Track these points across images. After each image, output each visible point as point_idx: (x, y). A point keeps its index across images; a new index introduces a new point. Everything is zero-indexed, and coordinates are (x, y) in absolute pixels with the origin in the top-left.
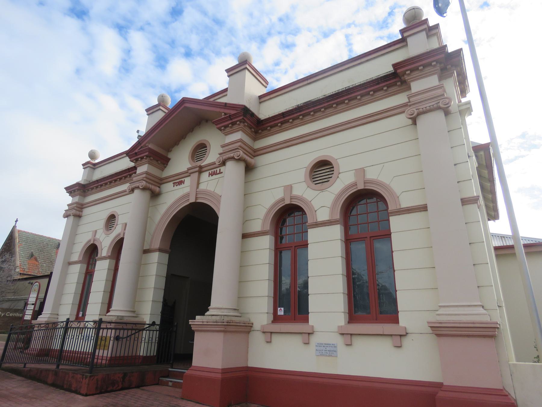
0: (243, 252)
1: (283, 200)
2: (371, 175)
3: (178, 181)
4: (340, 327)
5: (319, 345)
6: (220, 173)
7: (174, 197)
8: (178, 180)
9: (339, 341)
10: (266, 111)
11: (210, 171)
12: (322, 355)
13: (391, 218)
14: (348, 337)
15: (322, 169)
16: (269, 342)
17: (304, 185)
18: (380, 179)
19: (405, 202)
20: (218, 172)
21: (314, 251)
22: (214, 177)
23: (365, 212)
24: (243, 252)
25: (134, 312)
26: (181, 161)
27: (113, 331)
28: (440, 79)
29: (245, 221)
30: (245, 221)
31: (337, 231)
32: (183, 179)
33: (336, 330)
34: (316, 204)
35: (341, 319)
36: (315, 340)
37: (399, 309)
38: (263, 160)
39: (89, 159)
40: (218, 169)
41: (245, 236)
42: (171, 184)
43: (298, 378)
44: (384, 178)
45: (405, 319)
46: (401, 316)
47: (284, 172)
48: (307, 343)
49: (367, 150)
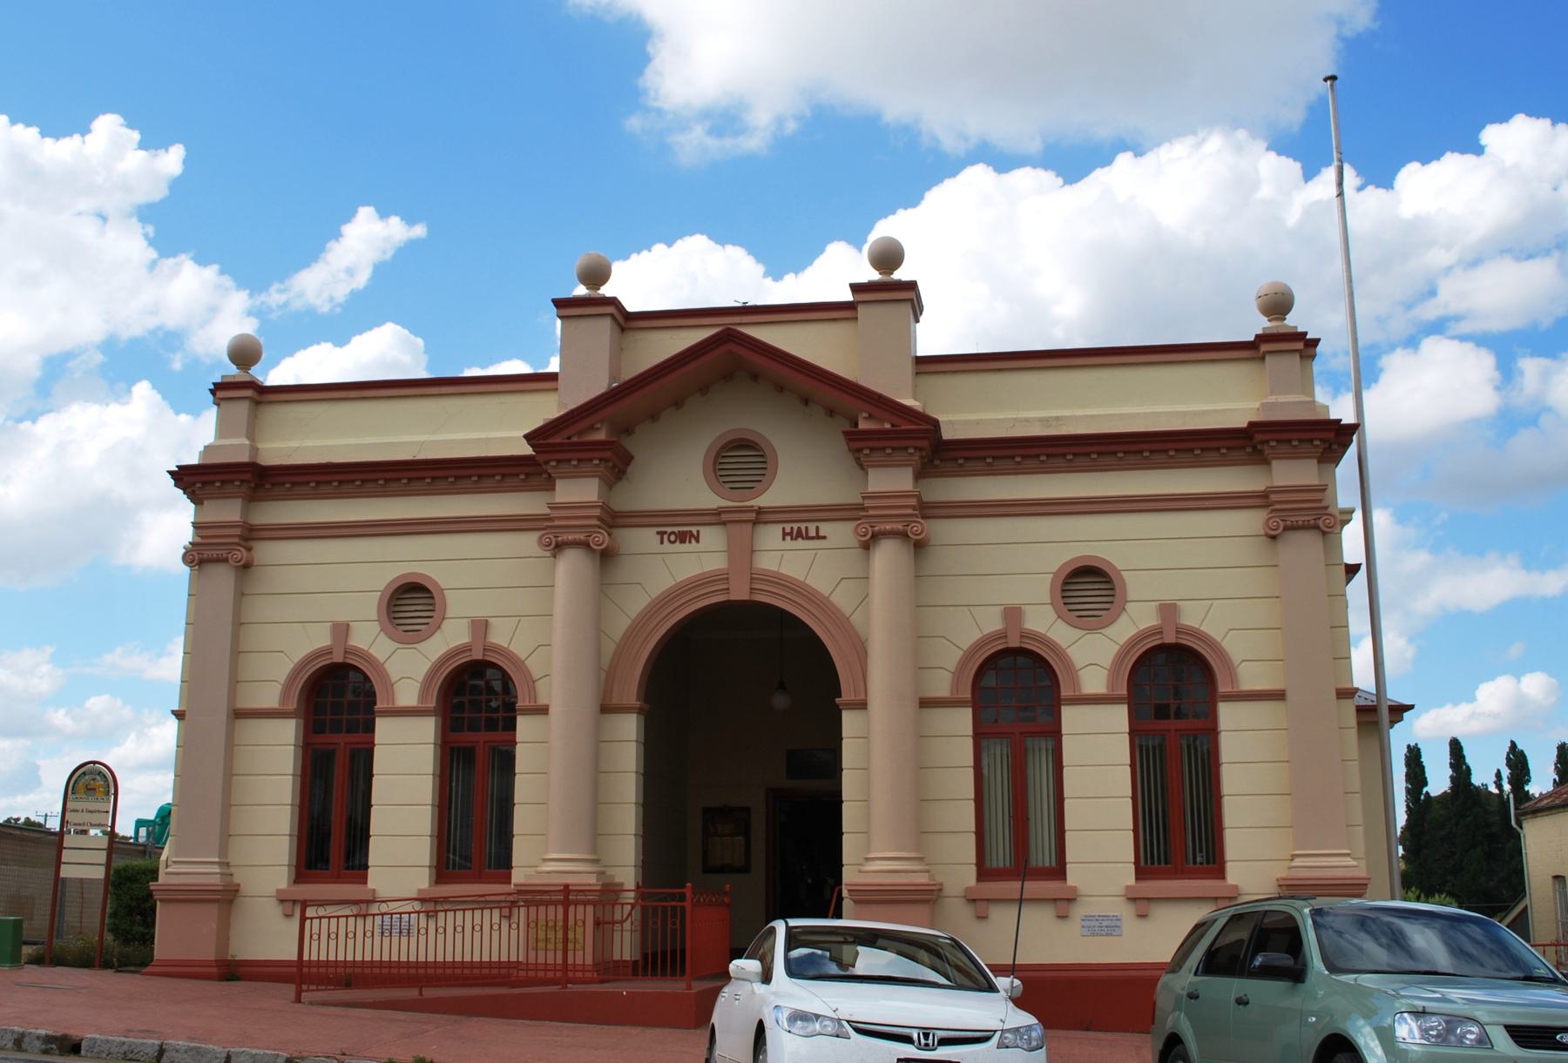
0: (921, 737)
1: (466, 649)
2: (1191, 617)
3: (676, 529)
4: (968, 889)
5: (1088, 918)
6: (818, 537)
7: (672, 572)
8: (680, 527)
9: (1126, 912)
10: (966, 414)
11: (788, 527)
12: (1093, 935)
13: (378, 721)
14: (1141, 903)
15: (1088, 585)
16: (982, 917)
17: (376, 627)
18: (452, 646)
19: (1251, 677)
20: (812, 533)
21: (383, 760)
22: (800, 543)
23: (1174, 687)
24: (921, 737)
25: (596, 861)
26: (677, 476)
27: (590, 909)
28: (919, 476)
29: (920, 668)
30: (920, 668)
31: (427, 729)
32: (694, 530)
33: (1122, 892)
34: (394, 669)
35: (1126, 875)
36: (1078, 911)
37: (844, 861)
38: (267, 552)
39: (232, 370)
40: (812, 528)
41: (239, 714)
42: (777, 530)
43: (1105, 974)
44: (1211, 629)
45: (378, 880)
46: (1231, 869)
47: (1003, 571)
48: (1063, 917)
49: (1189, 566)
